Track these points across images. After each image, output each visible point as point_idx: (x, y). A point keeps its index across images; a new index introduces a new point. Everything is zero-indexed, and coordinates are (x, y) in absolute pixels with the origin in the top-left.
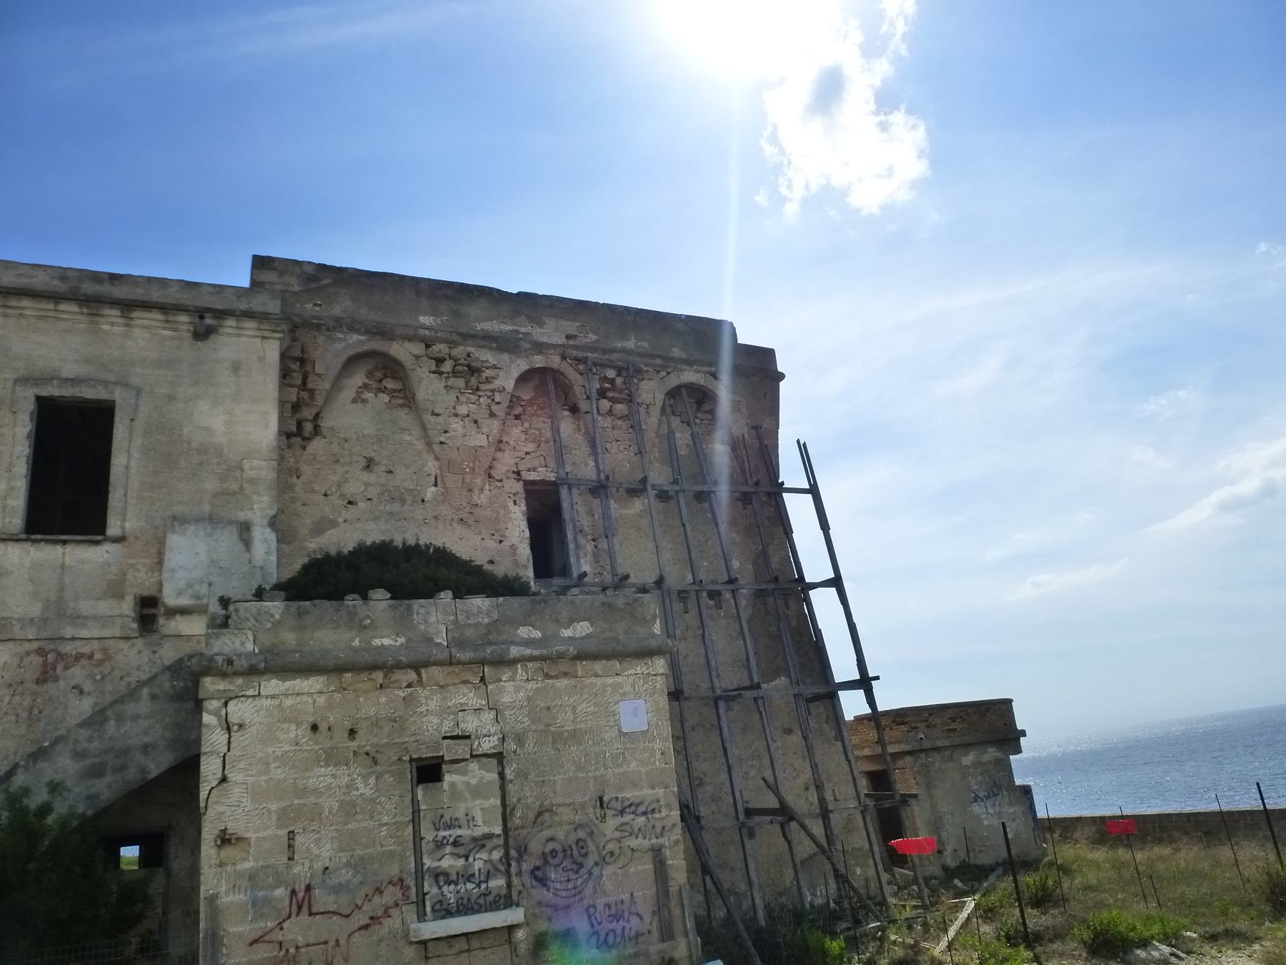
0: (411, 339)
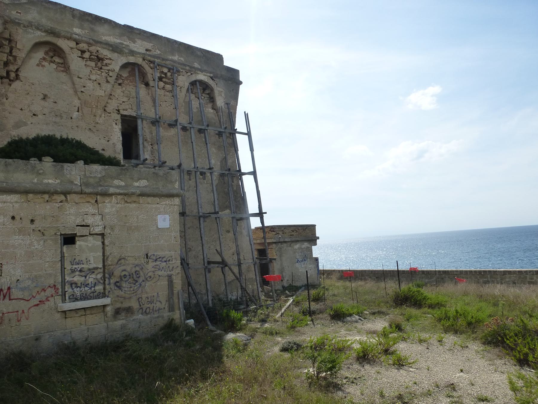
0: (69, 38)
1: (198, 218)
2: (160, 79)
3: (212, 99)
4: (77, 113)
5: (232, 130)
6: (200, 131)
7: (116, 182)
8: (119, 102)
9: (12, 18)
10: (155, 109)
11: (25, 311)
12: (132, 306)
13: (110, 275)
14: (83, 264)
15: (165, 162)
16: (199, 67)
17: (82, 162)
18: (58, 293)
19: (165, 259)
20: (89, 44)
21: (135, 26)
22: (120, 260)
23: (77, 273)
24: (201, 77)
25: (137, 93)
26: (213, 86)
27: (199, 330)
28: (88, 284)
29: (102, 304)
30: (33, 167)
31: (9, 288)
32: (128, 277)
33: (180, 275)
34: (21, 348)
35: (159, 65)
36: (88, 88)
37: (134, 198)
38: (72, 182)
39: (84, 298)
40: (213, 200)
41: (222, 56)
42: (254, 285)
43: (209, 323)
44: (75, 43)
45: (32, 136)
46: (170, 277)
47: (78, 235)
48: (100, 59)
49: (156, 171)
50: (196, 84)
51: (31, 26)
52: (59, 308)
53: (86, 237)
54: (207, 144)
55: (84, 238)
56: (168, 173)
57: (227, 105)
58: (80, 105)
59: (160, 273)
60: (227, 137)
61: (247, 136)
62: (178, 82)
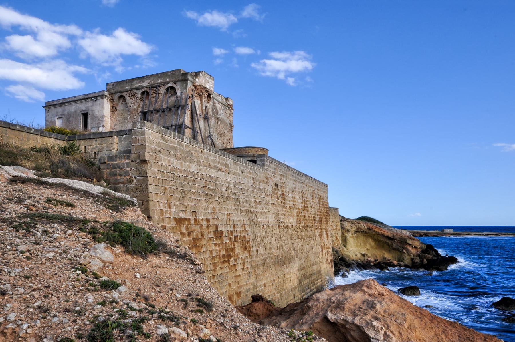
0: (125, 92)
24: (170, 85)
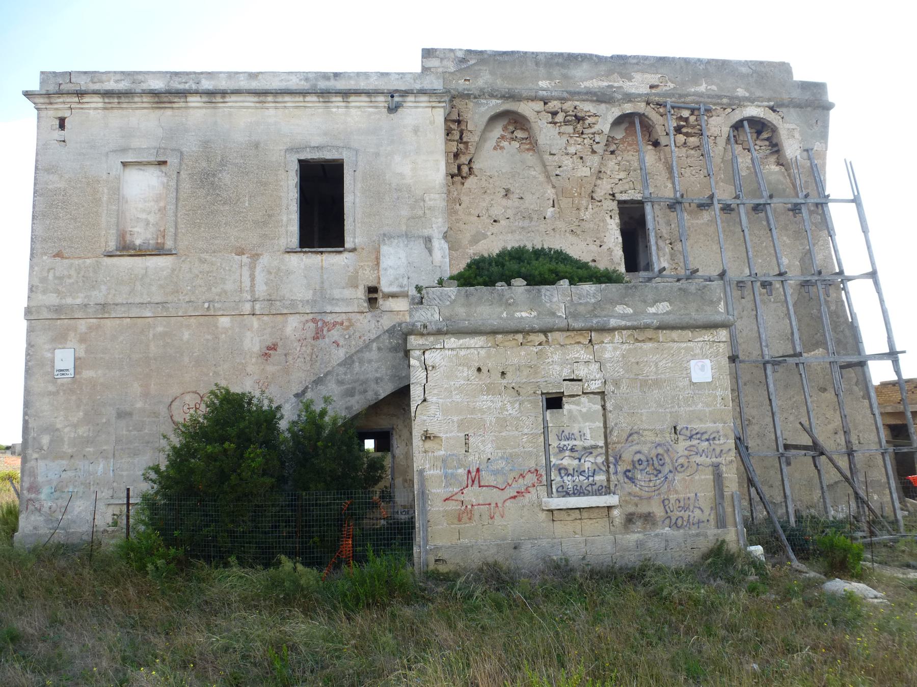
0: (533, 99)
1: (762, 365)
2: (678, 130)
3: (775, 148)
4: (552, 209)
5: (820, 197)
6: (757, 208)
7: (620, 309)
8: (613, 181)
9: (460, 89)
10: (673, 183)
11: (500, 505)
12: (653, 513)
13: (616, 459)
14: (575, 439)
15: (697, 270)
16: (747, 95)
17: (567, 281)
18: (541, 482)
19: (705, 436)
20: (563, 100)
21: (629, 53)
22: (630, 435)
23: (567, 453)
24: (752, 111)
25: (641, 161)
26: (775, 122)
27: (773, 566)
28: (584, 471)
29: (605, 505)
30: (501, 296)
31: (478, 470)
32: (645, 463)
33: (735, 465)
34: (496, 557)
35: (673, 108)
36: (565, 168)
37: (649, 333)
38: (553, 314)
39: (579, 492)
40: (790, 332)
41: (788, 64)
42: (884, 494)
43: (793, 556)
44: (542, 103)
45: (496, 251)
46: (716, 466)
47: (565, 394)
48: (579, 119)
49: (684, 286)
50: (742, 126)
51: (484, 95)
52: (543, 504)
53: (578, 398)
54: (771, 230)
55: (574, 399)
56: (705, 287)
57: (805, 153)
58: (555, 196)
59: (698, 459)
60: (811, 213)
61: (854, 204)
62: (709, 129)
